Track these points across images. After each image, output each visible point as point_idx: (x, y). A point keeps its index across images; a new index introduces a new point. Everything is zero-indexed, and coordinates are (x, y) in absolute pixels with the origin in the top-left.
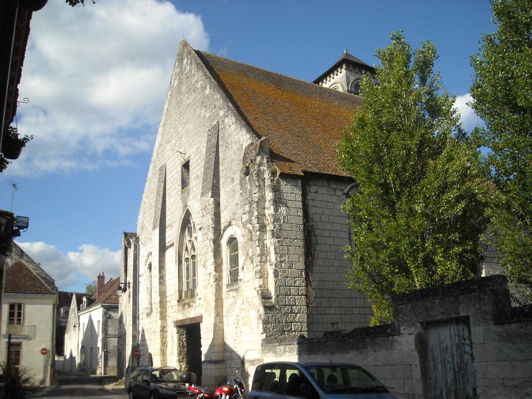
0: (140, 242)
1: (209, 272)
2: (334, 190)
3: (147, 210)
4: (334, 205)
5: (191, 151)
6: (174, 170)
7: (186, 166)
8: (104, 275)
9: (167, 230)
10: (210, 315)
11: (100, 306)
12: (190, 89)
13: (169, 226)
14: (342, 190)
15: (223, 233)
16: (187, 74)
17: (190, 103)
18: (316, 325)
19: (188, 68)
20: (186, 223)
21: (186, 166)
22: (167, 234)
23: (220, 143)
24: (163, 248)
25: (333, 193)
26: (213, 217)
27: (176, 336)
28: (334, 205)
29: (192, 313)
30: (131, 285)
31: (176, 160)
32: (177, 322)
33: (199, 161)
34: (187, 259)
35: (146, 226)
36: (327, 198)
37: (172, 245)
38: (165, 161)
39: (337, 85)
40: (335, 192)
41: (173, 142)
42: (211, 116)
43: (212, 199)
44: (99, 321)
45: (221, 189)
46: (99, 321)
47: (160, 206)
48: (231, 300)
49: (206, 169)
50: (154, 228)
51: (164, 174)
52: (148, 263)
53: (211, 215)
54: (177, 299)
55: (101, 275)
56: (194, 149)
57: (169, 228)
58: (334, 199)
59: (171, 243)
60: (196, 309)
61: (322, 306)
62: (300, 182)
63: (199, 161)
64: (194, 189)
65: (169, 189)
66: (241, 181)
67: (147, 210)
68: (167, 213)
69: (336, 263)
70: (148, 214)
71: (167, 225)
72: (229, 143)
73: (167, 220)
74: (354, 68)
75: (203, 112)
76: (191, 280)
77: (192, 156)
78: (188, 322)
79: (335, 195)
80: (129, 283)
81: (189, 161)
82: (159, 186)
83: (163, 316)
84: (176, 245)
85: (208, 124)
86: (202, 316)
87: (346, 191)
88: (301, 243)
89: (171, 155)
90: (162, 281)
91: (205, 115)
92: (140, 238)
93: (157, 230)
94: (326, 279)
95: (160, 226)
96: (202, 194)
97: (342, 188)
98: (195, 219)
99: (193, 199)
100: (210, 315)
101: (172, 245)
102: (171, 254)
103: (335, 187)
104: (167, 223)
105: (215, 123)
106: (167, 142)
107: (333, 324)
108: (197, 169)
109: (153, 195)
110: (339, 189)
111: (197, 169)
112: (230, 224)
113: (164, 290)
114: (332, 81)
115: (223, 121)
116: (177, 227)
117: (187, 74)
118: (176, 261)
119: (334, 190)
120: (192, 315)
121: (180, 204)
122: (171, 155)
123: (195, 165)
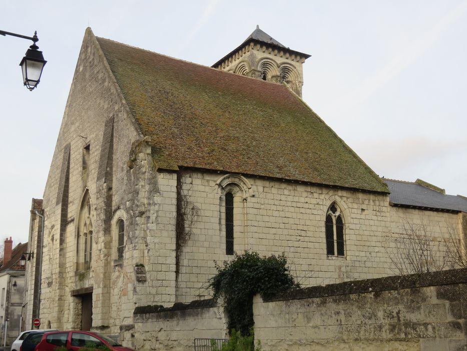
0: (45, 215)
1: (99, 248)
2: (208, 181)
3: (52, 184)
4: (207, 195)
5: (91, 136)
6: (77, 151)
7: (87, 148)
8: (12, 240)
9: (69, 206)
10: (99, 287)
11: (5, 273)
12: (93, 78)
13: (71, 202)
14: (215, 181)
15: (114, 215)
16: (90, 63)
17: (92, 91)
18: (184, 297)
19: (92, 57)
20: (85, 201)
21: (87, 148)
22: (69, 210)
23: (114, 134)
24: (65, 222)
25: (206, 184)
26: (105, 200)
27: (72, 305)
28: (207, 195)
29: (87, 284)
30: (35, 256)
31: (79, 142)
32: (73, 291)
33: (98, 147)
34: (86, 234)
35: (51, 200)
36: (202, 188)
37: (73, 220)
38: (70, 140)
39: (245, 63)
40: (209, 184)
41: (77, 124)
42: (108, 108)
43: (105, 184)
44: (4, 289)
45: (114, 175)
46: (4, 289)
47: (63, 183)
48: (117, 274)
49: (102, 156)
50: (57, 203)
51: (68, 153)
52: (51, 236)
53: (104, 198)
54: (75, 271)
55: (9, 239)
56: (94, 136)
57: (71, 204)
58: (207, 189)
59: (72, 218)
60: (90, 280)
61: (191, 280)
62: (175, 176)
63: (98, 147)
64: (93, 171)
65: (55, 194)
66: (127, 172)
67: (52, 184)
68: (70, 190)
69: (206, 244)
70: (53, 188)
71: (69, 202)
72: (122, 136)
73: (69, 196)
74: (261, 47)
75: (102, 102)
76: (88, 254)
77: (92, 141)
78: (84, 292)
79: (208, 185)
80: (33, 253)
81: (89, 145)
82: (64, 164)
83: (62, 285)
84: (76, 221)
85: (106, 115)
86: (93, 287)
87: (218, 182)
88: (174, 228)
89: (74, 136)
90: (266, 178)
91: (103, 105)
92: (46, 210)
93: (60, 206)
94: (195, 258)
95: (62, 202)
96: (98, 179)
97: (216, 179)
98: (93, 200)
99: (92, 180)
100: (99, 287)
101: (73, 220)
102: (71, 229)
103: (208, 178)
104: (70, 199)
105: (111, 115)
106: (72, 124)
107: (200, 296)
108: (96, 154)
109: (58, 171)
110: (212, 180)
111: (96, 154)
112: (119, 208)
113: (64, 262)
114: (241, 59)
115: (117, 115)
116: (77, 205)
117: (90, 63)
118: (75, 236)
119: (208, 181)
120: (87, 286)
121: (80, 184)
122: (74, 136)
123: (94, 149)
